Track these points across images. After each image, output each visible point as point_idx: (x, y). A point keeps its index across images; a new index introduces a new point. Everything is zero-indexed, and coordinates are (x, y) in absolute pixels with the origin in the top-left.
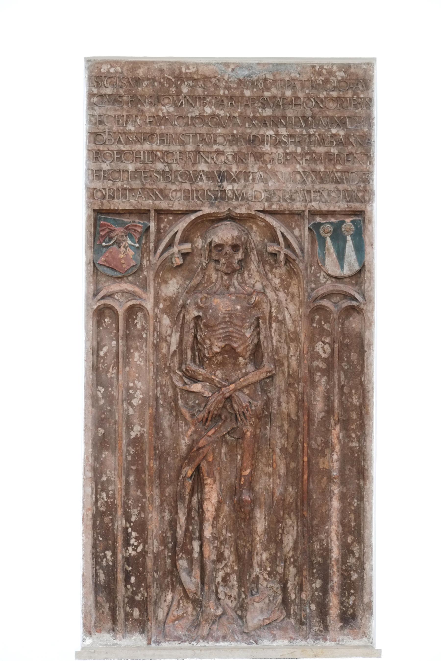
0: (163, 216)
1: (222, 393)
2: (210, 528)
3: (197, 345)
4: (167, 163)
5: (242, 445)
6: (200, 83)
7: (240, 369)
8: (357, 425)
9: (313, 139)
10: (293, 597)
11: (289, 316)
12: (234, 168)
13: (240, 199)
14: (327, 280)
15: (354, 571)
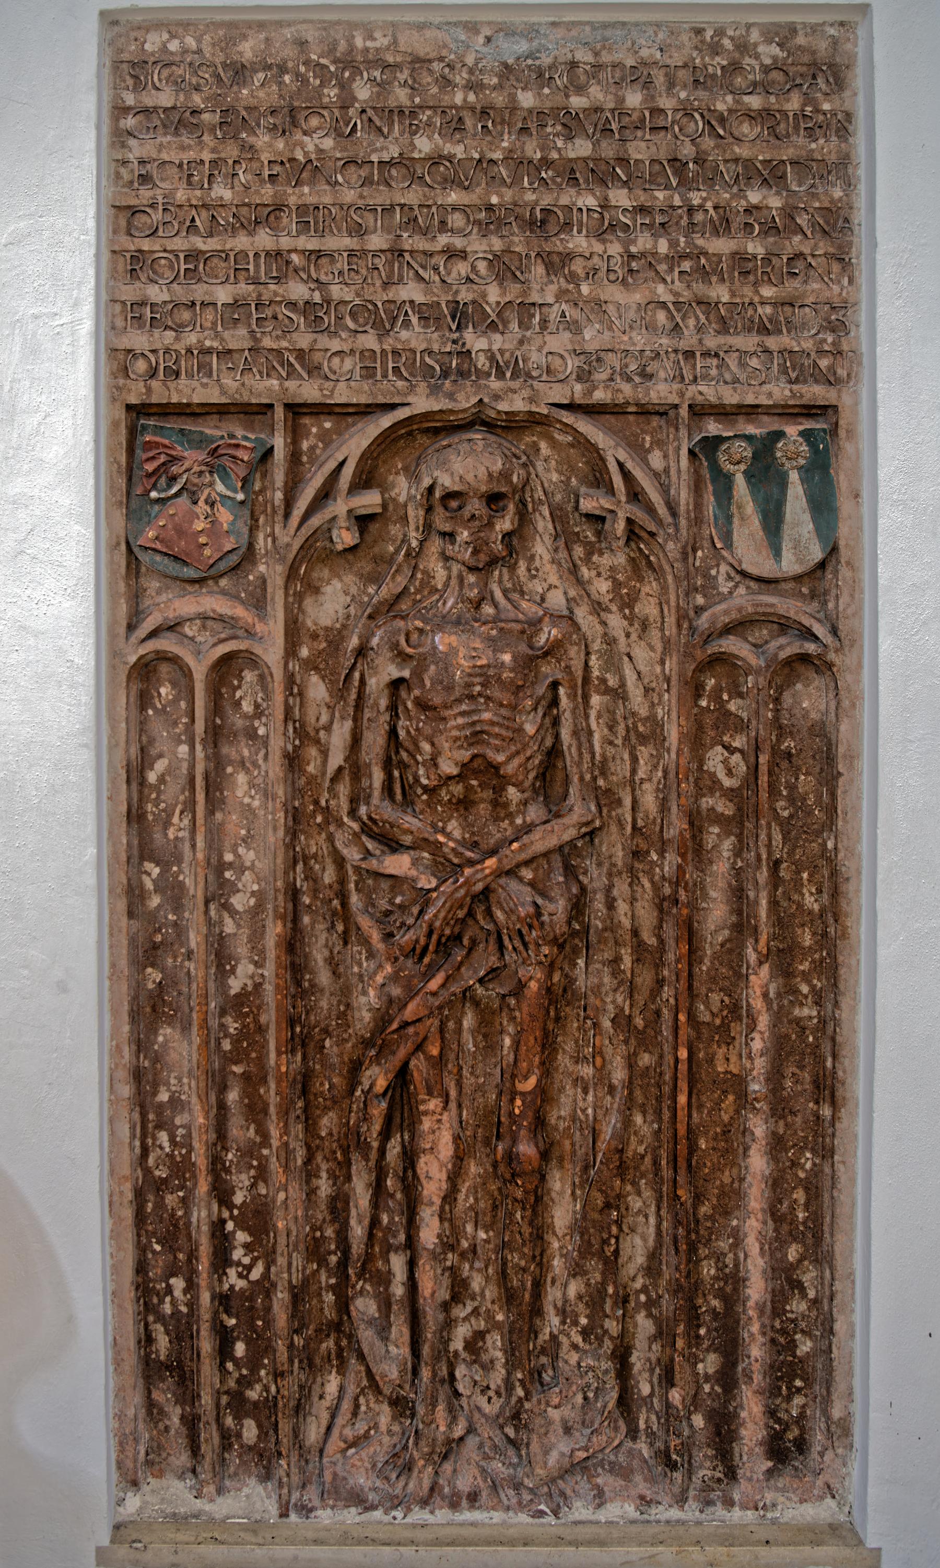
0: (306, 421)
1: (465, 883)
2: (436, 1222)
3: (397, 753)
4: (317, 281)
5: (517, 1014)
6: (403, 76)
7: (510, 816)
8: (813, 961)
9: (699, 217)
10: (646, 1389)
11: (635, 677)
12: (494, 294)
13: (508, 375)
14: (736, 586)
15: (802, 1331)
